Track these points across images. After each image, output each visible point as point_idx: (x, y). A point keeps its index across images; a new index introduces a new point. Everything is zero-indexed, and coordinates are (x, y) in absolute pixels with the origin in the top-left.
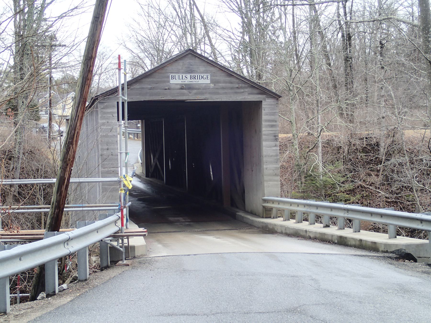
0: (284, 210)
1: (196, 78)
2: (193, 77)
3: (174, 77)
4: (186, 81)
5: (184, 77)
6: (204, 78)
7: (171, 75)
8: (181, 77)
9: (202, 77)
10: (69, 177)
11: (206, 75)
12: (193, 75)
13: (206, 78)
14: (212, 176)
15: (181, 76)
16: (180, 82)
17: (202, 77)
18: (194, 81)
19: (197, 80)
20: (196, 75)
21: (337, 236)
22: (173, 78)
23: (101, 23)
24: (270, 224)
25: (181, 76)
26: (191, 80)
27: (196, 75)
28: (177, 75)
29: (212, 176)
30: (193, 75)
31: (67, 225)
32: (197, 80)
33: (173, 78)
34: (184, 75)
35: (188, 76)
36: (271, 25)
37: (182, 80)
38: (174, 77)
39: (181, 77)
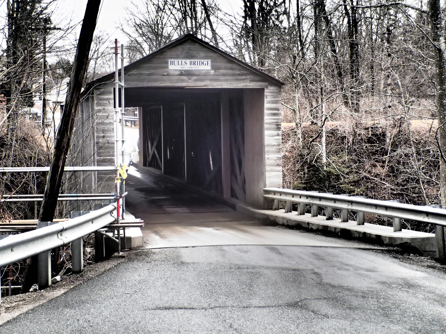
1: (196, 64)
3: (173, 63)
5: (183, 63)
6: (204, 64)
7: (170, 60)
9: (203, 63)
11: (206, 61)
12: (193, 61)
13: (206, 64)
17: (203, 63)
19: (197, 66)
22: (191, 64)
26: (191, 66)
27: (196, 61)
31: (61, 215)
33: (191, 64)
35: (188, 61)
38: (173, 63)
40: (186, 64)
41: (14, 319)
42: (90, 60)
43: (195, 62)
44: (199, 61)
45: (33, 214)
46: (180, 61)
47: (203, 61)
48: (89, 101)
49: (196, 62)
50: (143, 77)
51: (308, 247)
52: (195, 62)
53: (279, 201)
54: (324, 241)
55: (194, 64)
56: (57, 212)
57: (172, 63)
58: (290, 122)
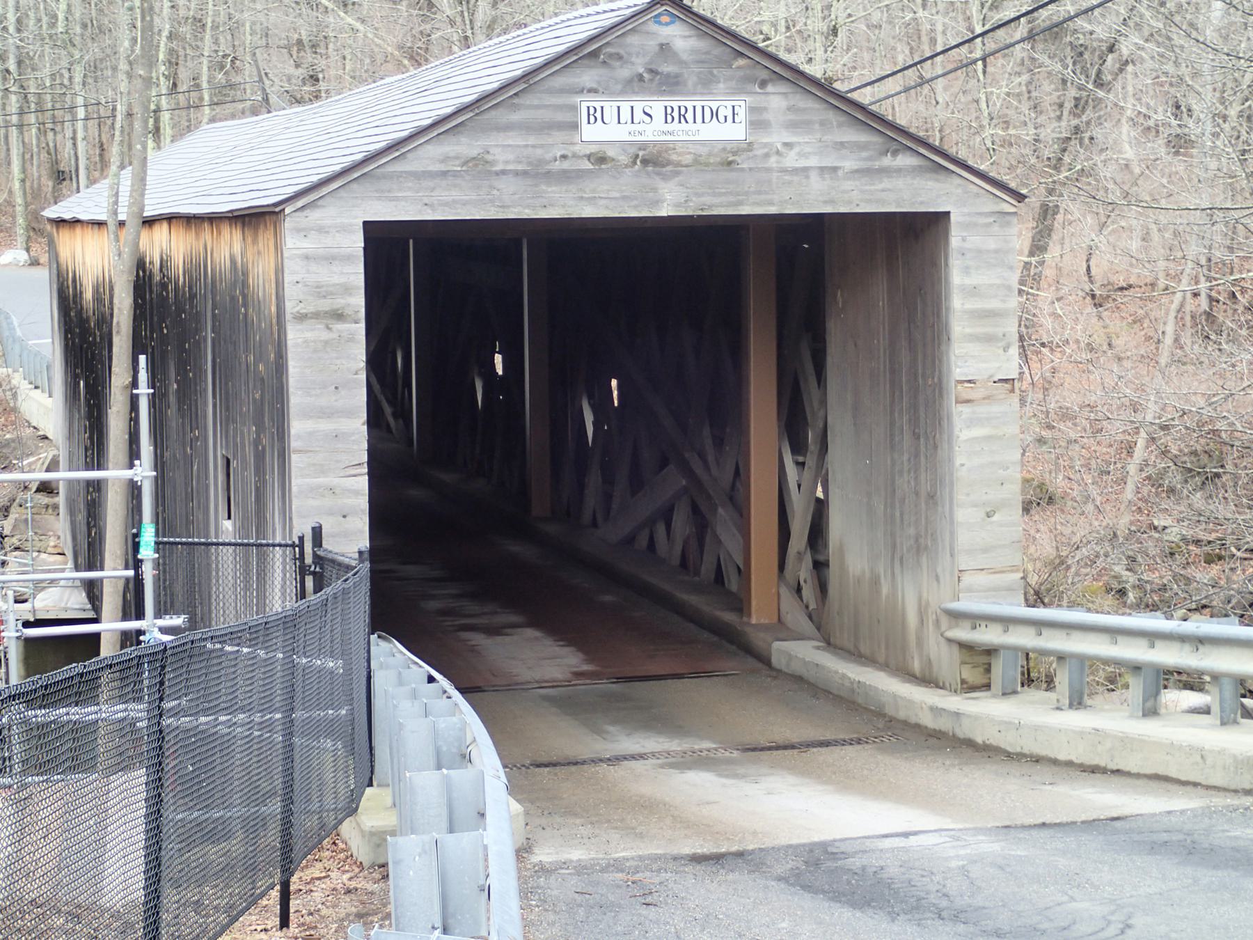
1: (689, 116)
2: (676, 114)
3: (598, 115)
5: (639, 115)
6: (722, 119)
7: (584, 105)
9: (715, 114)
11: (729, 104)
13: (730, 119)
14: (615, 393)
17: (715, 114)
18: (681, 132)
19: (691, 126)
20: (699, 105)
21: (1235, 757)
23: (1154, 784)
24: (911, 702)
26: (669, 127)
27: (689, 105)
29: (615, 393)
31: (120, 479)
35: (657, 108)
37: (633, 127)
38: (598, 115)
40: (647, 119)
43: (683, 112)
48: (93, 287)
49: (676, 110)
50: (234, 830)
51: (1134, 770)
52: (683, 112)
55: (682, 117)
57: (592, 116)
58: (209, 82)
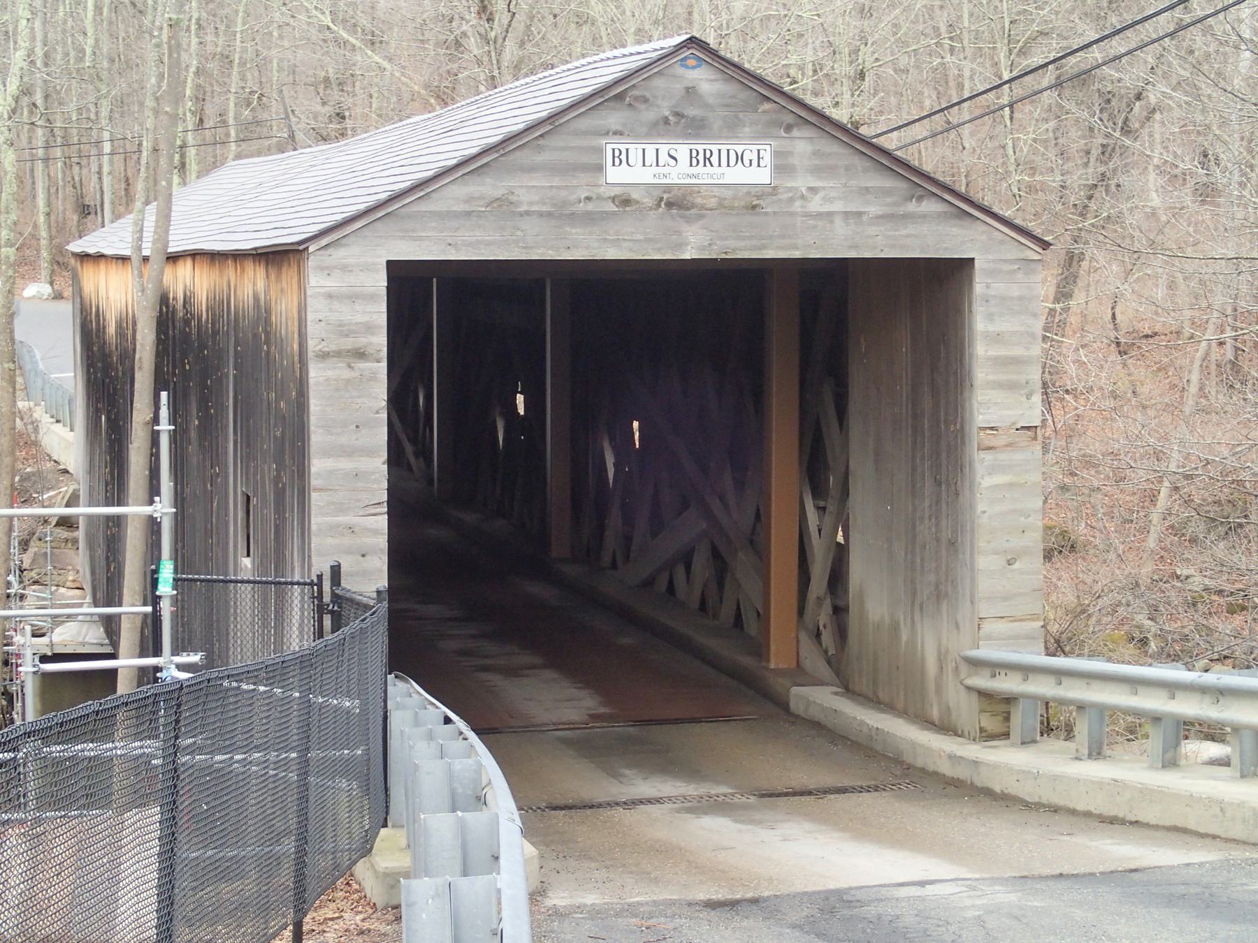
0: (1163, 767)
1: (715, 160)
2: (701, 158)
3: (623, 157)
4: (674, 175)
5: (664, 158)
6: (747, 162)
7: (609, 147)
8: (651, 157)
9: (740, 158)
10: (75, 376)
11: (755, 148)
12: (700, 148)
13: (755, 163)
15: (651, 150)
16: (645, 176)
17: (740, 158)
18: (706, 175)
19: (716, 169)
20: (724, 148)
22: (694, 161)
25: (664, 150)
27: (715, 148)
28: (635, 150)
30: (700, 148)
31: (140, 516)
32: (719, 170)
33: (694, 161)
34: (664, 150)
35: (682, 151)
36: (278, 42)
37: (655, 170)
38: (623, 157)
39: (651, 157)
40: (672, 162)
41: (1073, 875)
42: (826, 593)
44: (724, 148)
45: (114, 501)
46: (651, 150)
47: (740, 149)
53: (1178, 722)
54: (913, 744)
55: (707, 160)
56: (386, 596)
